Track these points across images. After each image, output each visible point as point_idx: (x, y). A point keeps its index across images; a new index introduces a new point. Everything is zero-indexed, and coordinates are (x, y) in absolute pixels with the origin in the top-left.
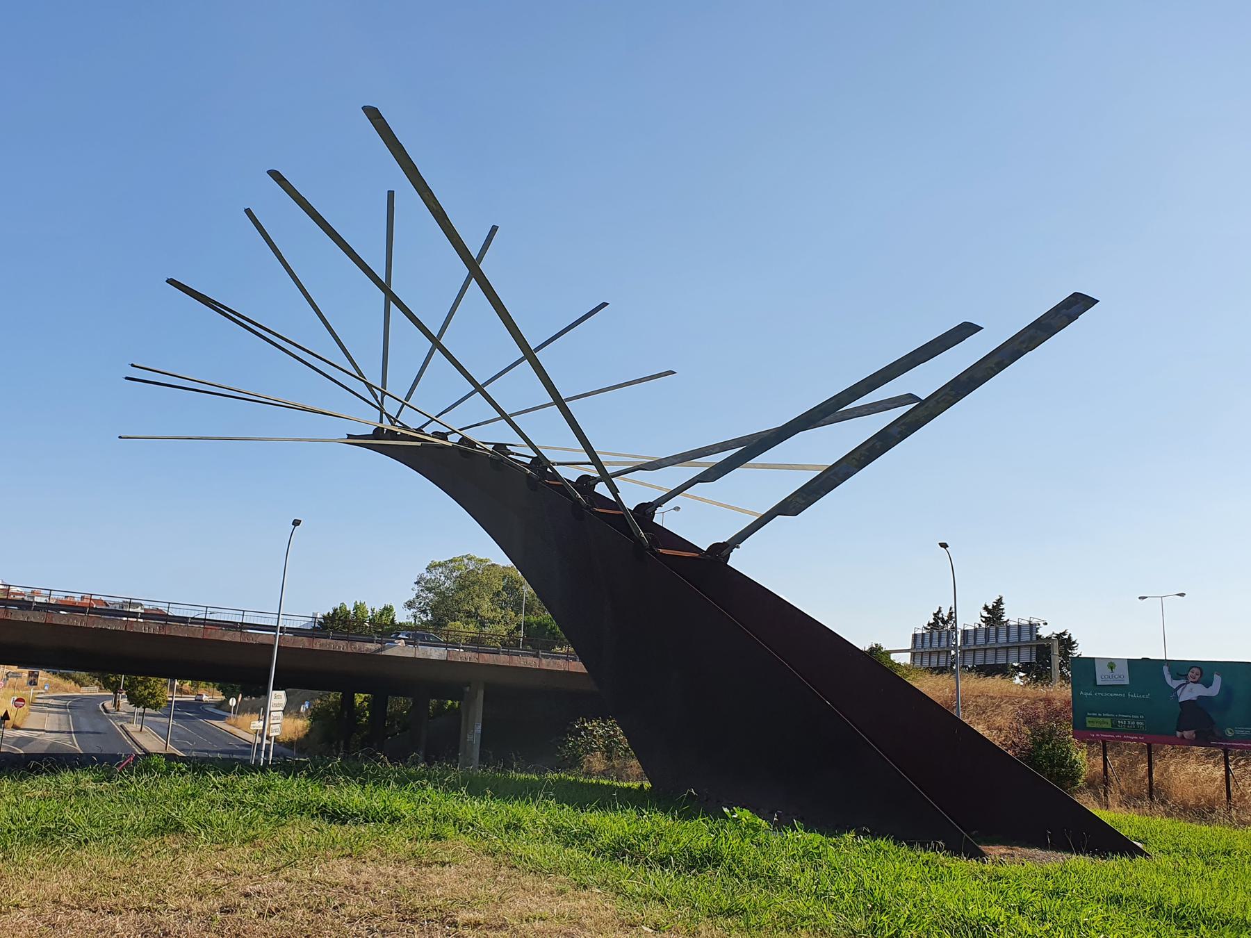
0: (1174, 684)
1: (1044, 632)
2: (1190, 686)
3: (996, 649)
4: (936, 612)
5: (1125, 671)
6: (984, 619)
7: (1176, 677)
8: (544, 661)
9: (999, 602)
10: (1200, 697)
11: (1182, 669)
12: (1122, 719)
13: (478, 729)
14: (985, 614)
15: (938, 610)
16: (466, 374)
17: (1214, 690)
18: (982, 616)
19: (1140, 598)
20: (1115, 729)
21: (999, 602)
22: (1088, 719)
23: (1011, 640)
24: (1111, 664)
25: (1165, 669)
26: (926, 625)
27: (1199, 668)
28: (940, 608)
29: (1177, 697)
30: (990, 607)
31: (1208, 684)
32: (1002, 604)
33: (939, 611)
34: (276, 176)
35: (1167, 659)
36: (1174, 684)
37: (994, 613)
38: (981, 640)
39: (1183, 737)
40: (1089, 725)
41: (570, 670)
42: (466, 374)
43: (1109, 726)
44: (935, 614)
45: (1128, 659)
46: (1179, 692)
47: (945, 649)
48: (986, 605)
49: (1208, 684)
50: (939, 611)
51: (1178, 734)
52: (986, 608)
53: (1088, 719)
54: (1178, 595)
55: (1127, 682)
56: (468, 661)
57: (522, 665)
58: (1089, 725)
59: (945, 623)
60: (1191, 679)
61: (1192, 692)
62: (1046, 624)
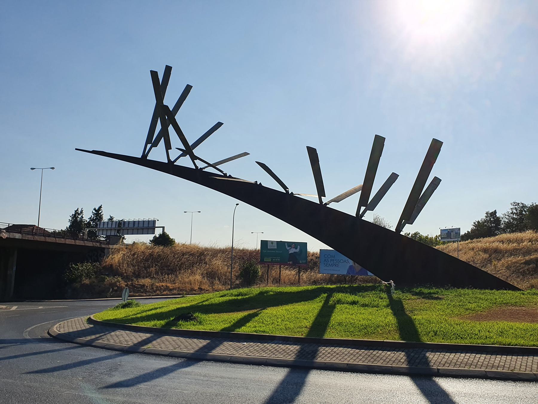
0: (288, 248)
1: (125, 221)
2: (292, 249)
3: (128, 229)
4: (76, 210)
5: (275, 244)
6: (93, 214)
7: (289, 246)
8: (57, 239)
9: (100, 207)
10: (294, 252)
11: (290, 244)
12: (274, 258)
13: (15, 268)
14: (94, 212)
15: (77, 209)
16: (219, 163)
17: (298, 250)
18: (93, 212)
19: (184, 212)
20: (272, 262)
21: (100, 207)
22: (265, 259)
23: (145, 226)
24: (272, 242)
25: (286, 244)
26: (71, 215)
27: (295, 244)
28: (78, 208)
29: (289, 252)
30: (97, 209)
31: (296, 249)
32: (102, 208)
33: (77, 210)
34: (313, 153)
35: (39, 227)
36: (288, 248)
37: (98, 213)
38: (106, 226)
39: (289, 263)
40: (265, 260)
41: (67, 243)
42: (219, 163)
43: (270, 261)
44: (75, 211)
45: (277, 241)
46: (289, 250)
47: (106, 229)
48: (95, 208)
49: (296, 249)
50: (77, 210)
51: (288, 262)
52: (95, 209)
53: (265, 259)
54: (198, 212)
55: (276, 248)
56: (30, 239)
57: (50, 241)
58: (265, 260)
59: (79, 214)
60: (292, 247)
61: (292, 251)
62: (158, 220)
